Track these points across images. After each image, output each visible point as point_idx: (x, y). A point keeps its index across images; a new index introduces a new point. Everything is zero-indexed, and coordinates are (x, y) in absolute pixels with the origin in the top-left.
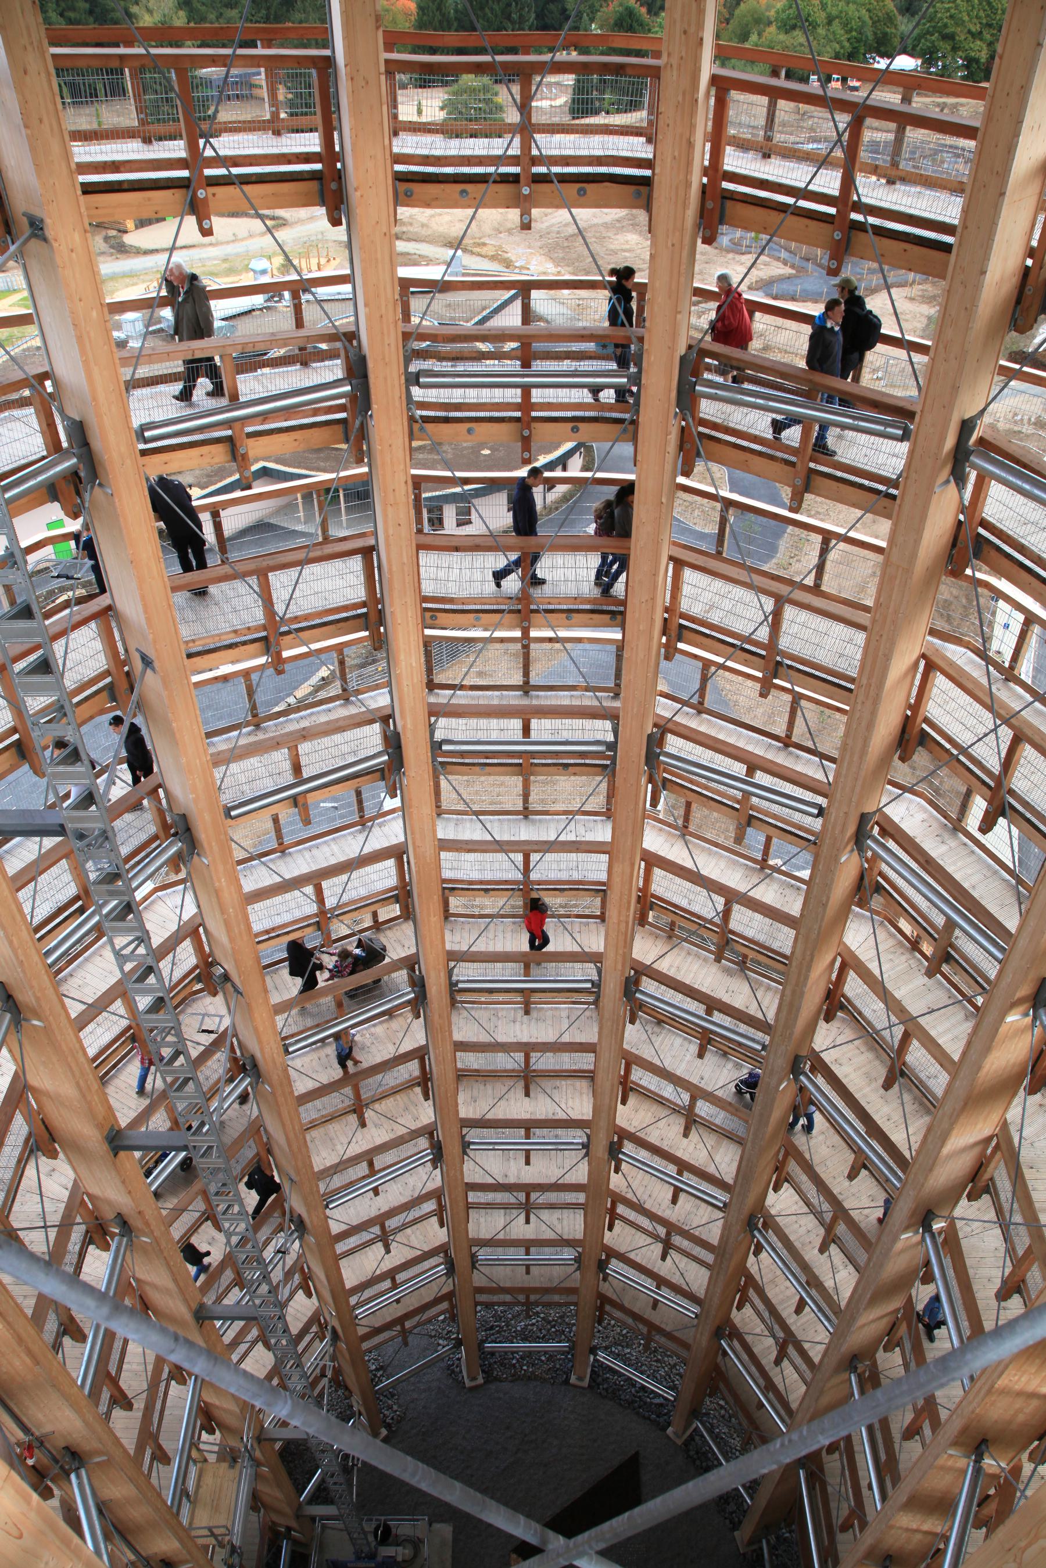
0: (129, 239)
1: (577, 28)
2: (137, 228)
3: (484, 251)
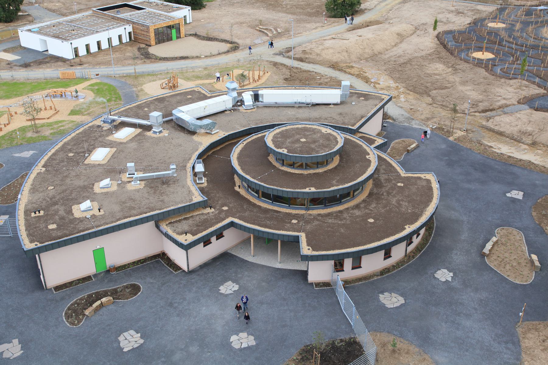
2: (156, 44)
3: (352, 71)
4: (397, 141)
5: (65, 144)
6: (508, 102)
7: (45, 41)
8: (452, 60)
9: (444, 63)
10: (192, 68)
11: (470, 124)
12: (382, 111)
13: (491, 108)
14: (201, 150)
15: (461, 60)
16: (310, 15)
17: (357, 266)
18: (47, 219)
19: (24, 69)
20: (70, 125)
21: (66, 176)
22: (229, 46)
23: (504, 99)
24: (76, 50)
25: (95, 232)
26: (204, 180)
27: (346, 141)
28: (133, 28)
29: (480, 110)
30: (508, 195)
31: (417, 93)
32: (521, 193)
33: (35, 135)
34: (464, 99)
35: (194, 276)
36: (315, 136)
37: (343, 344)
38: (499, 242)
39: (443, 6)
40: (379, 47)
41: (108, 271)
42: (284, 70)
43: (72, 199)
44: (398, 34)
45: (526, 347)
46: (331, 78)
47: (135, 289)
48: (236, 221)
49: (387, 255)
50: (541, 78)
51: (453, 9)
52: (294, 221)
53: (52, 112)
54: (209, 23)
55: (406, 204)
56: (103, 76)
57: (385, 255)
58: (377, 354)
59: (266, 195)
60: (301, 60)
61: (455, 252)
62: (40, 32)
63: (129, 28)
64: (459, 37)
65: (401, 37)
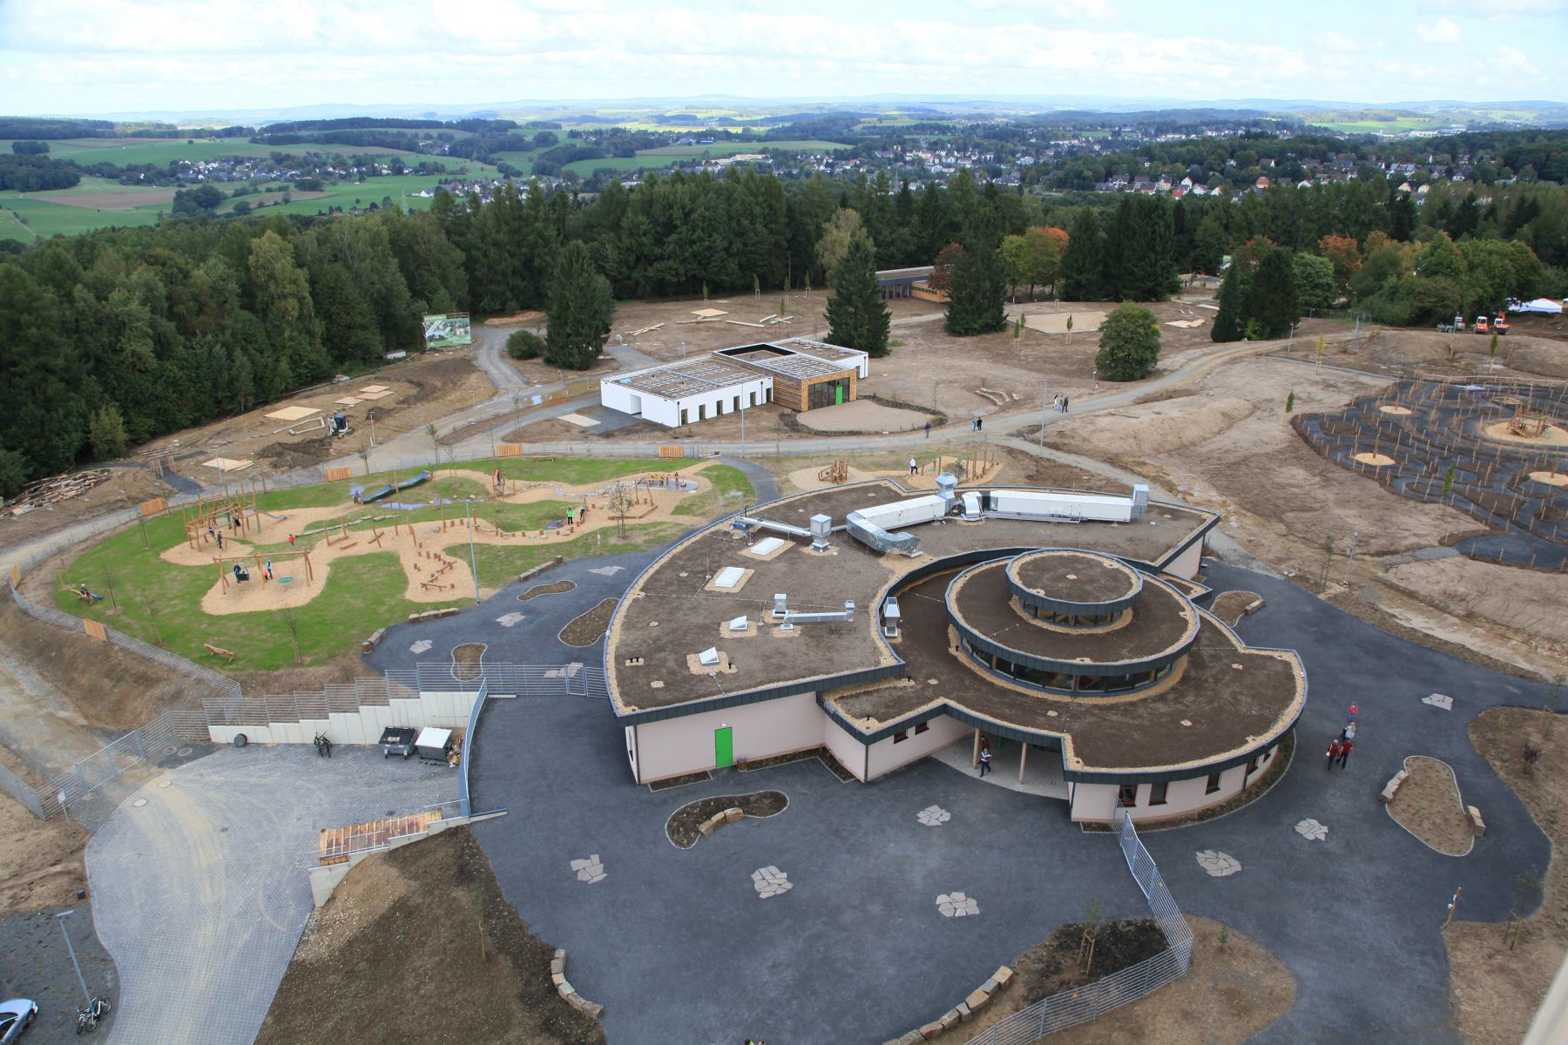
0: (806, 418)
1: (1490, 487)
2: (809, 409)
3: (1145, 470)
4: (1225, 593)
5: (674, 557)
6: (1423, 542)
7: (639, 399)
8: (1321, 463)
9: (1306, 468)
10: (870, 449)
11: (1354, 573)
12: (1200, 541)
13: (1392, 549)
14: (892, 582)
15: (1336, 464)
16: (1068, 374)
17: (1158, 799)
18: (650, 671)
19: (604, 441)
20: (674, 530)
21: (677, 608)
22: (929, 418)
23: (1415, 535)
24: (684, 414)
25: (723, 700)
26: (897, 633)
27: (1146, 584)
28: (775, 382)
29: (1372, 551)
30: (1426, 701)
31: (1260, 515)
32: (1449, 700)
33: (621, 542)
34: (1344, 530)
35: (874, 790)
36: (1091, 572)
37: (1132, 928)
38: (1411, 781)
39: (1299, 372)
40: (1191, 433)
41: (735, 768)
42: (1027, 461)
43: (686, 645)
44: (1224, 414)
45: (1458, 964)
46: (1108, 479)
47: (778, 801)
48: (953, 704)
49: (1213, 787)
50: (1478, 505)
51: (1318, 378)
52: (1052, 713)
53: (647, 508)
54: (896, 380)
55: (1249, 700)
56: (726, 456)
57: (1209, 785)
58: (1192, 952)
59: (1003, 665)
60: (1055, 447)
61: (1331, 791)
62: (633, 384)
63: (768, 383)
64: (1331, 426)
65: (1230, 420)
